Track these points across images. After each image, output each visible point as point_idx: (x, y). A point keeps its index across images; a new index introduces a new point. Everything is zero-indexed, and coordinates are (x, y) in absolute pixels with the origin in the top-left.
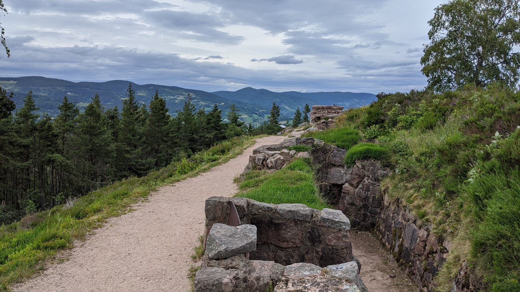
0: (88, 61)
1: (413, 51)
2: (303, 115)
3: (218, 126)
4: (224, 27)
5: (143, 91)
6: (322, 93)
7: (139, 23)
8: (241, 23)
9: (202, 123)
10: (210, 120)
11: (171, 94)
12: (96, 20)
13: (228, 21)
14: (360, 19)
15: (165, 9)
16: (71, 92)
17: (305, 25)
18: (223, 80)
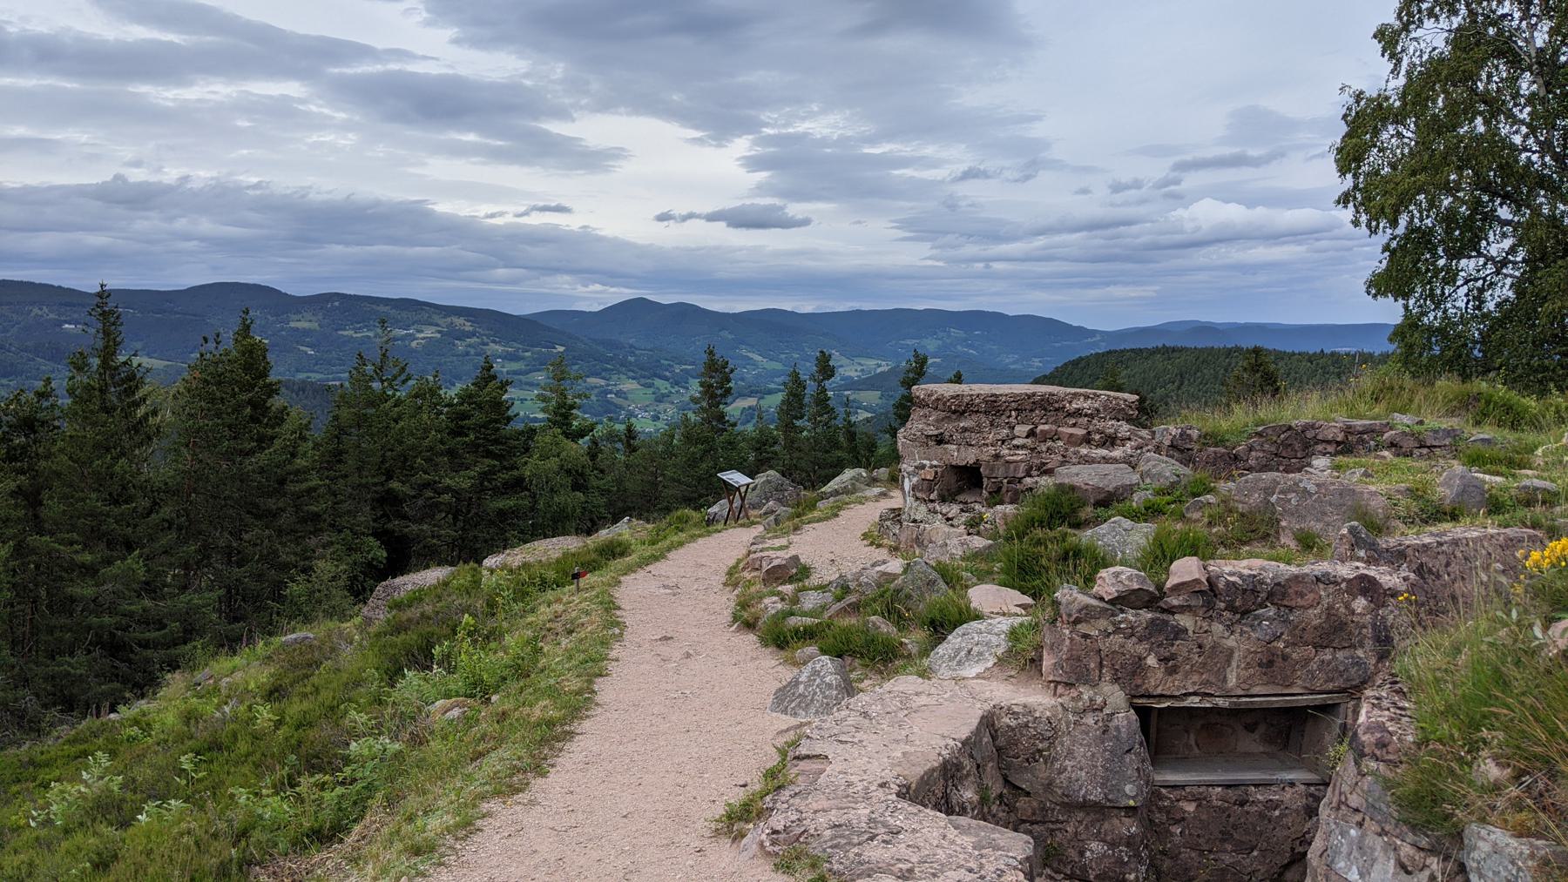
0: (146, 223)
1: (1127, 187)
2: (811, 388)
3: (496, 442)
4: (573, 120)
5: (308, 316)
6: (859, 312)
7: (314, 108)
8: (622, 109)
9: (426, 431)
10: (465, 416)
12: (174, 100)
13: (584, 102)
14: (971, 98)
15: (394, 66)
17: (811, 116)
18: (567, 278)
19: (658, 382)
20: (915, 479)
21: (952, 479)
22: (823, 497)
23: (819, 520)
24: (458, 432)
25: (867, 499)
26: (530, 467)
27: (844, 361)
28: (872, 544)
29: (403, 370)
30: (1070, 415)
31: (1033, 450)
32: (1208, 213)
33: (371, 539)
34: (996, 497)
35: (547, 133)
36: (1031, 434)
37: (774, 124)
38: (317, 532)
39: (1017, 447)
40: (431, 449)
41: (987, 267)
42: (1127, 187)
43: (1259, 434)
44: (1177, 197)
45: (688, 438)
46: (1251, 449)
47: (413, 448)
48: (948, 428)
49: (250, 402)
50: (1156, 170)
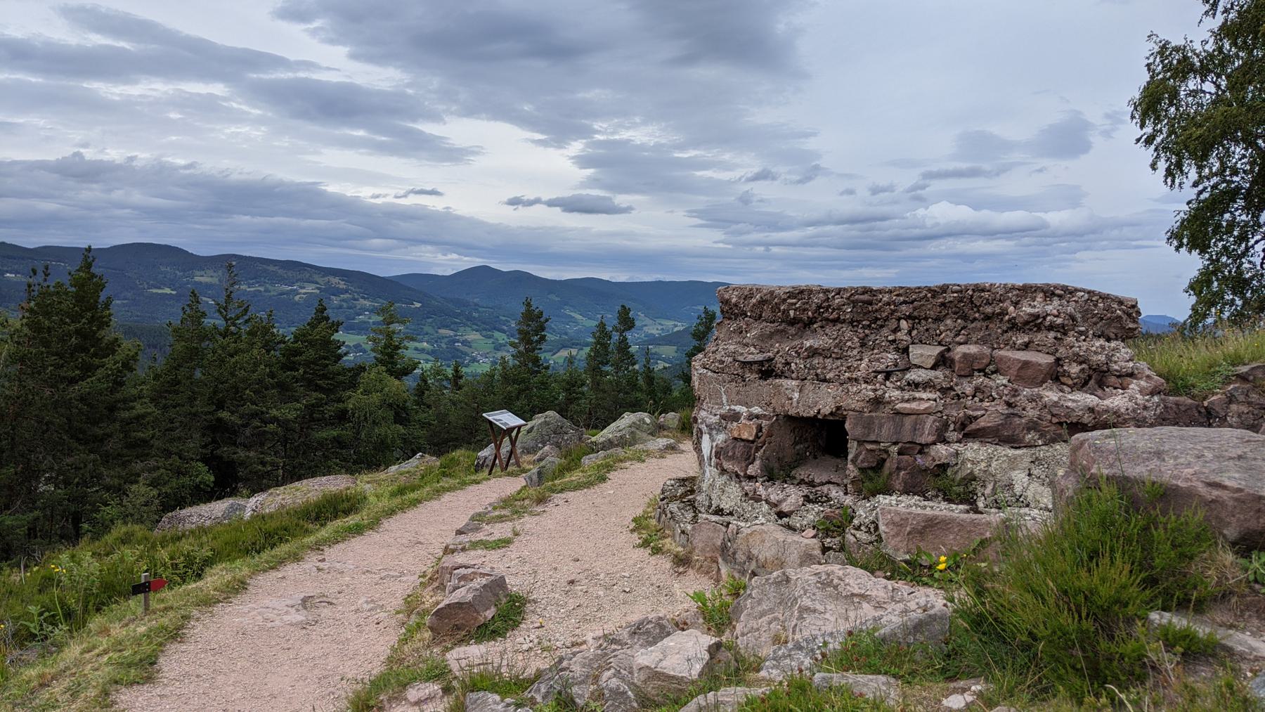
0: (91, 193)
1: (883, 190)
2: (616, 337)
3: (324, 377)
5: (210, 272)
7: (235, 105)
9: (256, 365)
10: (297, 353)
11: (283, 280)
12: (120, 95)
13: (454, 108)
14: (761, 117)
15: (302, 75)
16: (16, 272)
17: (634, 126)
18: (429, 248)
19: (497, 334)
20: (721, 438)
21: (786, 439)
22: (594, 448)
23: (578, 487)
24: (292, 367)
25: (648, 454)
26: (354, 400)
27: (648, 321)
28: (645, 544)
29: (246, 310)
30: (1014, 326)
31: (944, 391)
32: (942, 213)
33: (200, 464)
34: (873, 481)
35: (421, 133)
36: (943, 361)
37: (603, 130)
38: (143, 457)
39: (915, 385)
40: (260, 382)
41: (768, 250)
42: (883, 190)
43: (1243, 378)
44: (920, 199)
45: (505, 377)
46: (1231, 399)
47: (244, 380)
48: (781, 349)
49: (77, 332)
50: (905, 180)
